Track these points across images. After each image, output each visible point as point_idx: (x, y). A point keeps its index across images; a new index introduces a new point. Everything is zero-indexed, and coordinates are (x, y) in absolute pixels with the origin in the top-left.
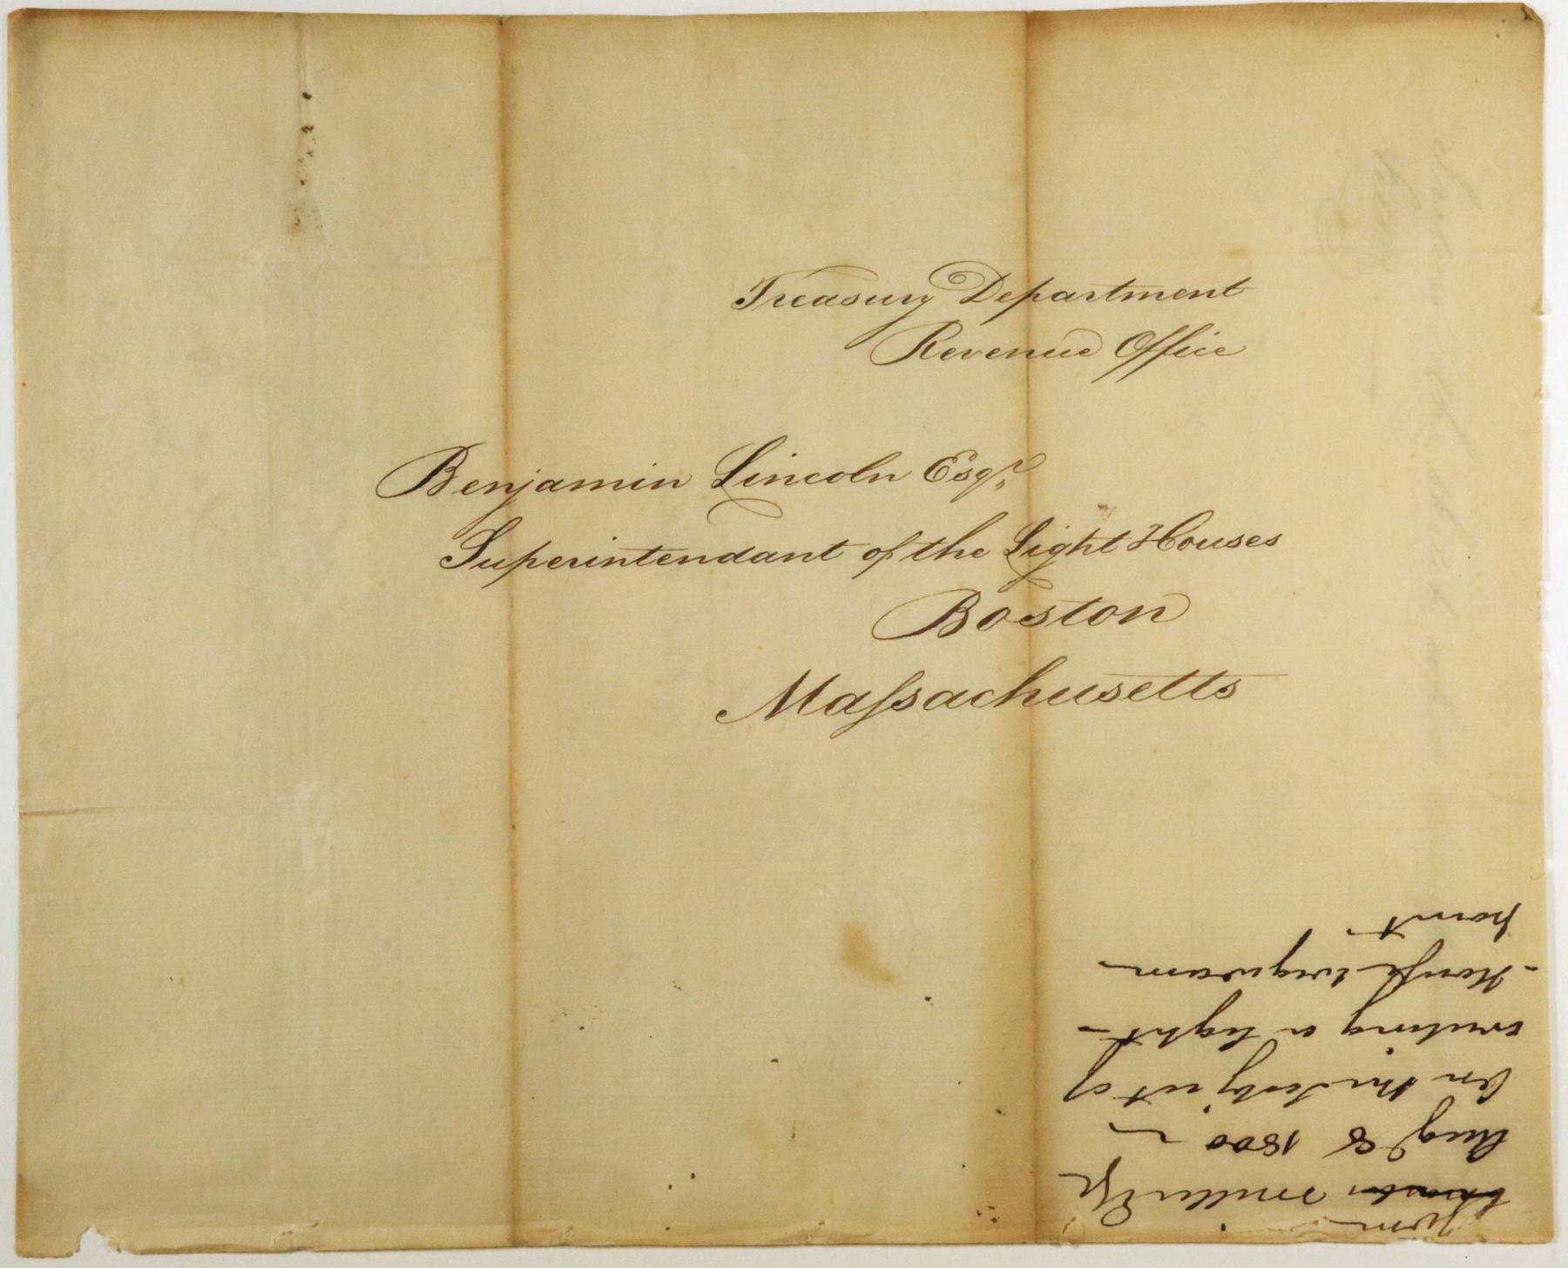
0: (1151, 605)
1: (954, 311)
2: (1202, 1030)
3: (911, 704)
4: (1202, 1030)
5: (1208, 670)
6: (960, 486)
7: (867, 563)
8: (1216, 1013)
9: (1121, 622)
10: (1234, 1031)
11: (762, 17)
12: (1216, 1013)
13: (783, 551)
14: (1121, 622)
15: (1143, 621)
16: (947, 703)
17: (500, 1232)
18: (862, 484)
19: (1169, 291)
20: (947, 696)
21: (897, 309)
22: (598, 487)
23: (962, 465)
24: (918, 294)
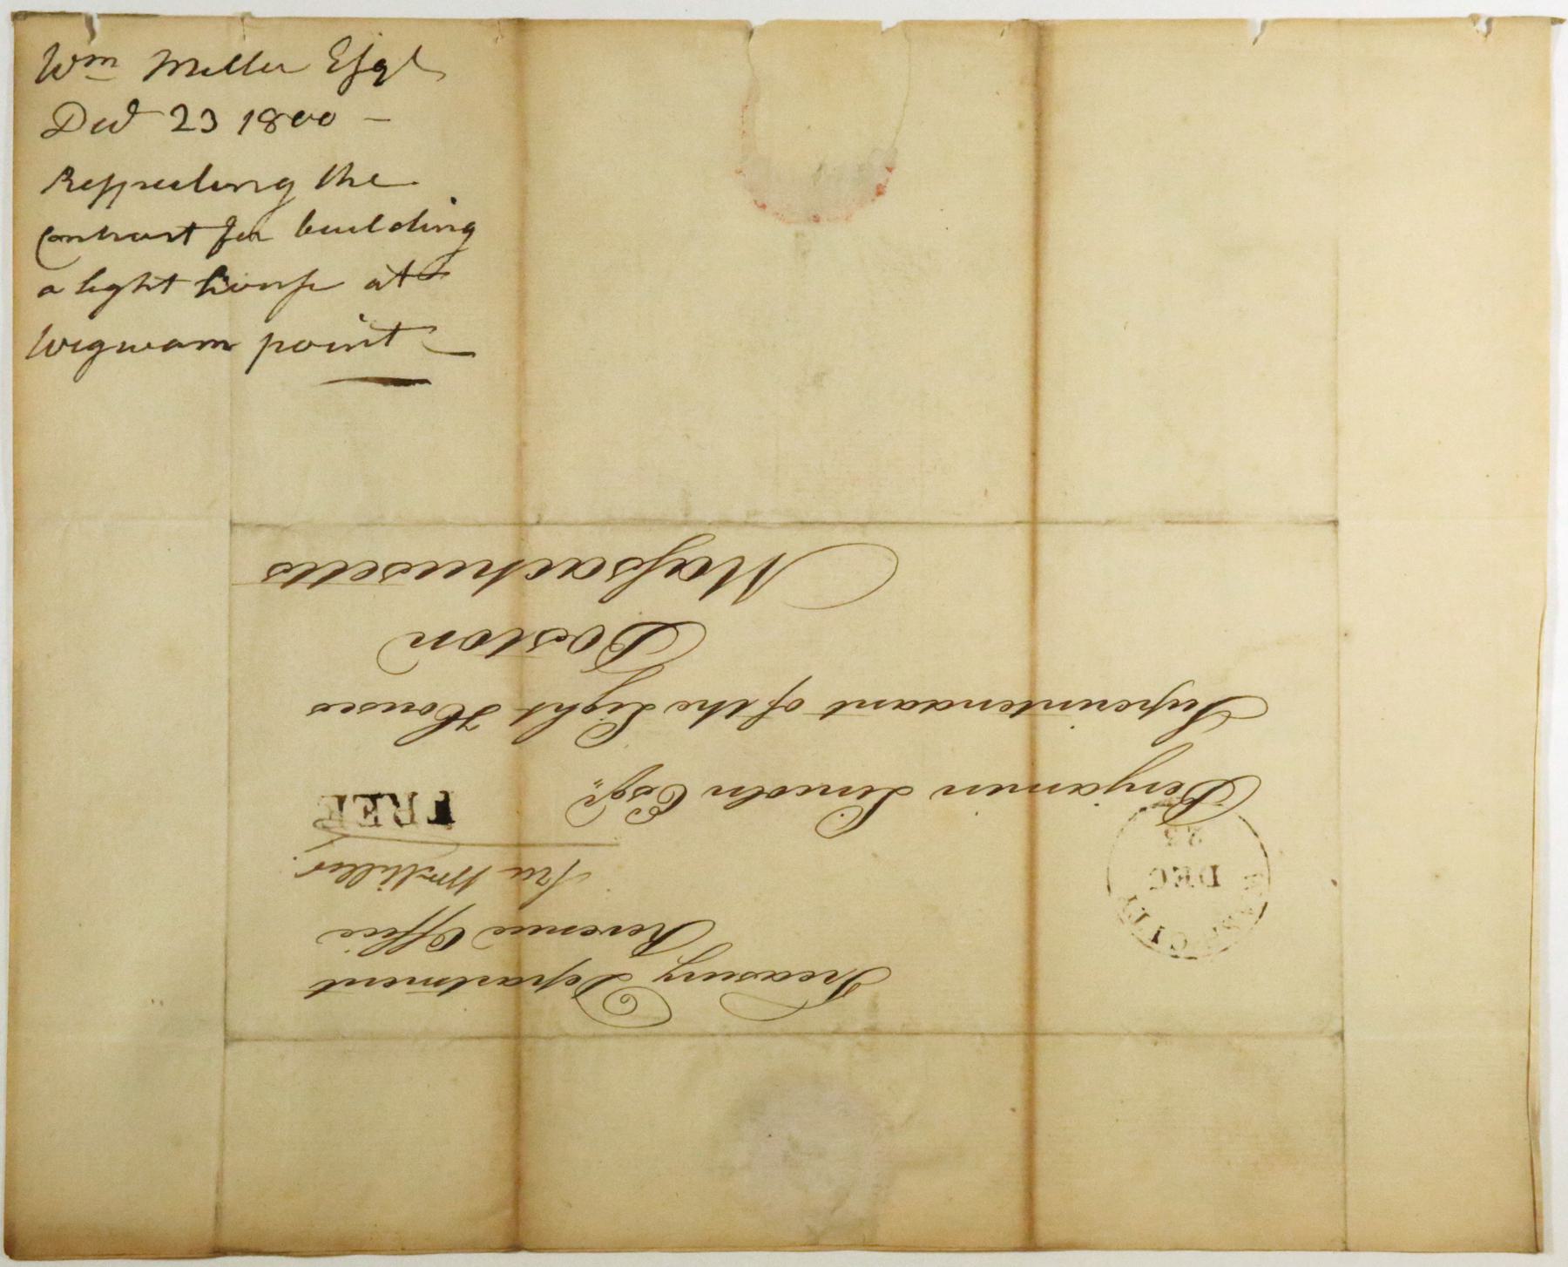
0: (425, 649)
1: (633, 965)
2: (115, 289)
3: (619, 565)
4: (115, 289)
5: (300, 587)
6: (650, 781)
7: (796, 695)
8: (105, 304)
9: (452, 633)
10: (91, 290)
11: (582, 1249)
12: (105, 304)
13: (885, 711)
14: (452, 633)
15: (433, 634)
16: (579, 564)
17: (1058, 40)
18: (750, 785)
19: (401, 987)
20: (580, 572)
21: (698, 969)
22: (995, 791)
23: (646, 802)
24: (678, 985)
